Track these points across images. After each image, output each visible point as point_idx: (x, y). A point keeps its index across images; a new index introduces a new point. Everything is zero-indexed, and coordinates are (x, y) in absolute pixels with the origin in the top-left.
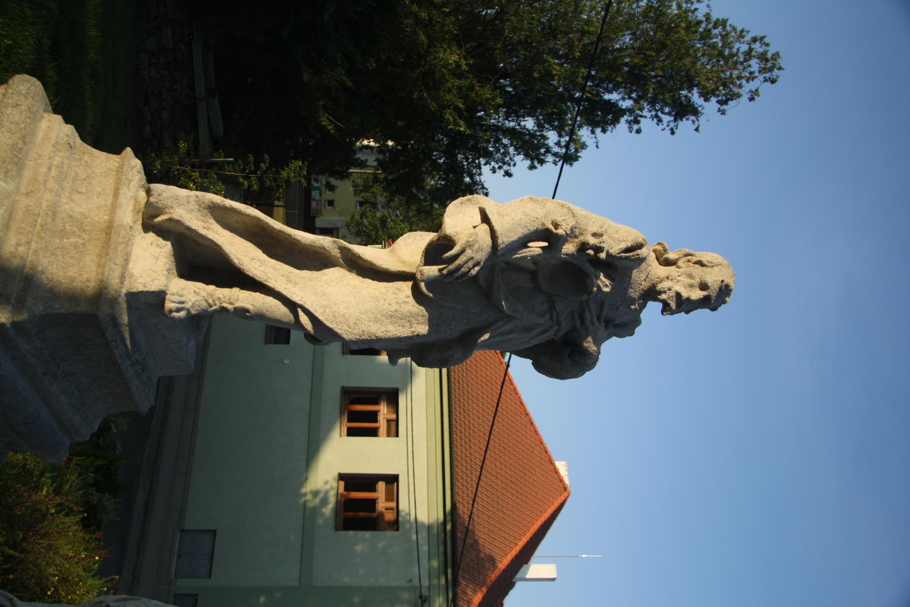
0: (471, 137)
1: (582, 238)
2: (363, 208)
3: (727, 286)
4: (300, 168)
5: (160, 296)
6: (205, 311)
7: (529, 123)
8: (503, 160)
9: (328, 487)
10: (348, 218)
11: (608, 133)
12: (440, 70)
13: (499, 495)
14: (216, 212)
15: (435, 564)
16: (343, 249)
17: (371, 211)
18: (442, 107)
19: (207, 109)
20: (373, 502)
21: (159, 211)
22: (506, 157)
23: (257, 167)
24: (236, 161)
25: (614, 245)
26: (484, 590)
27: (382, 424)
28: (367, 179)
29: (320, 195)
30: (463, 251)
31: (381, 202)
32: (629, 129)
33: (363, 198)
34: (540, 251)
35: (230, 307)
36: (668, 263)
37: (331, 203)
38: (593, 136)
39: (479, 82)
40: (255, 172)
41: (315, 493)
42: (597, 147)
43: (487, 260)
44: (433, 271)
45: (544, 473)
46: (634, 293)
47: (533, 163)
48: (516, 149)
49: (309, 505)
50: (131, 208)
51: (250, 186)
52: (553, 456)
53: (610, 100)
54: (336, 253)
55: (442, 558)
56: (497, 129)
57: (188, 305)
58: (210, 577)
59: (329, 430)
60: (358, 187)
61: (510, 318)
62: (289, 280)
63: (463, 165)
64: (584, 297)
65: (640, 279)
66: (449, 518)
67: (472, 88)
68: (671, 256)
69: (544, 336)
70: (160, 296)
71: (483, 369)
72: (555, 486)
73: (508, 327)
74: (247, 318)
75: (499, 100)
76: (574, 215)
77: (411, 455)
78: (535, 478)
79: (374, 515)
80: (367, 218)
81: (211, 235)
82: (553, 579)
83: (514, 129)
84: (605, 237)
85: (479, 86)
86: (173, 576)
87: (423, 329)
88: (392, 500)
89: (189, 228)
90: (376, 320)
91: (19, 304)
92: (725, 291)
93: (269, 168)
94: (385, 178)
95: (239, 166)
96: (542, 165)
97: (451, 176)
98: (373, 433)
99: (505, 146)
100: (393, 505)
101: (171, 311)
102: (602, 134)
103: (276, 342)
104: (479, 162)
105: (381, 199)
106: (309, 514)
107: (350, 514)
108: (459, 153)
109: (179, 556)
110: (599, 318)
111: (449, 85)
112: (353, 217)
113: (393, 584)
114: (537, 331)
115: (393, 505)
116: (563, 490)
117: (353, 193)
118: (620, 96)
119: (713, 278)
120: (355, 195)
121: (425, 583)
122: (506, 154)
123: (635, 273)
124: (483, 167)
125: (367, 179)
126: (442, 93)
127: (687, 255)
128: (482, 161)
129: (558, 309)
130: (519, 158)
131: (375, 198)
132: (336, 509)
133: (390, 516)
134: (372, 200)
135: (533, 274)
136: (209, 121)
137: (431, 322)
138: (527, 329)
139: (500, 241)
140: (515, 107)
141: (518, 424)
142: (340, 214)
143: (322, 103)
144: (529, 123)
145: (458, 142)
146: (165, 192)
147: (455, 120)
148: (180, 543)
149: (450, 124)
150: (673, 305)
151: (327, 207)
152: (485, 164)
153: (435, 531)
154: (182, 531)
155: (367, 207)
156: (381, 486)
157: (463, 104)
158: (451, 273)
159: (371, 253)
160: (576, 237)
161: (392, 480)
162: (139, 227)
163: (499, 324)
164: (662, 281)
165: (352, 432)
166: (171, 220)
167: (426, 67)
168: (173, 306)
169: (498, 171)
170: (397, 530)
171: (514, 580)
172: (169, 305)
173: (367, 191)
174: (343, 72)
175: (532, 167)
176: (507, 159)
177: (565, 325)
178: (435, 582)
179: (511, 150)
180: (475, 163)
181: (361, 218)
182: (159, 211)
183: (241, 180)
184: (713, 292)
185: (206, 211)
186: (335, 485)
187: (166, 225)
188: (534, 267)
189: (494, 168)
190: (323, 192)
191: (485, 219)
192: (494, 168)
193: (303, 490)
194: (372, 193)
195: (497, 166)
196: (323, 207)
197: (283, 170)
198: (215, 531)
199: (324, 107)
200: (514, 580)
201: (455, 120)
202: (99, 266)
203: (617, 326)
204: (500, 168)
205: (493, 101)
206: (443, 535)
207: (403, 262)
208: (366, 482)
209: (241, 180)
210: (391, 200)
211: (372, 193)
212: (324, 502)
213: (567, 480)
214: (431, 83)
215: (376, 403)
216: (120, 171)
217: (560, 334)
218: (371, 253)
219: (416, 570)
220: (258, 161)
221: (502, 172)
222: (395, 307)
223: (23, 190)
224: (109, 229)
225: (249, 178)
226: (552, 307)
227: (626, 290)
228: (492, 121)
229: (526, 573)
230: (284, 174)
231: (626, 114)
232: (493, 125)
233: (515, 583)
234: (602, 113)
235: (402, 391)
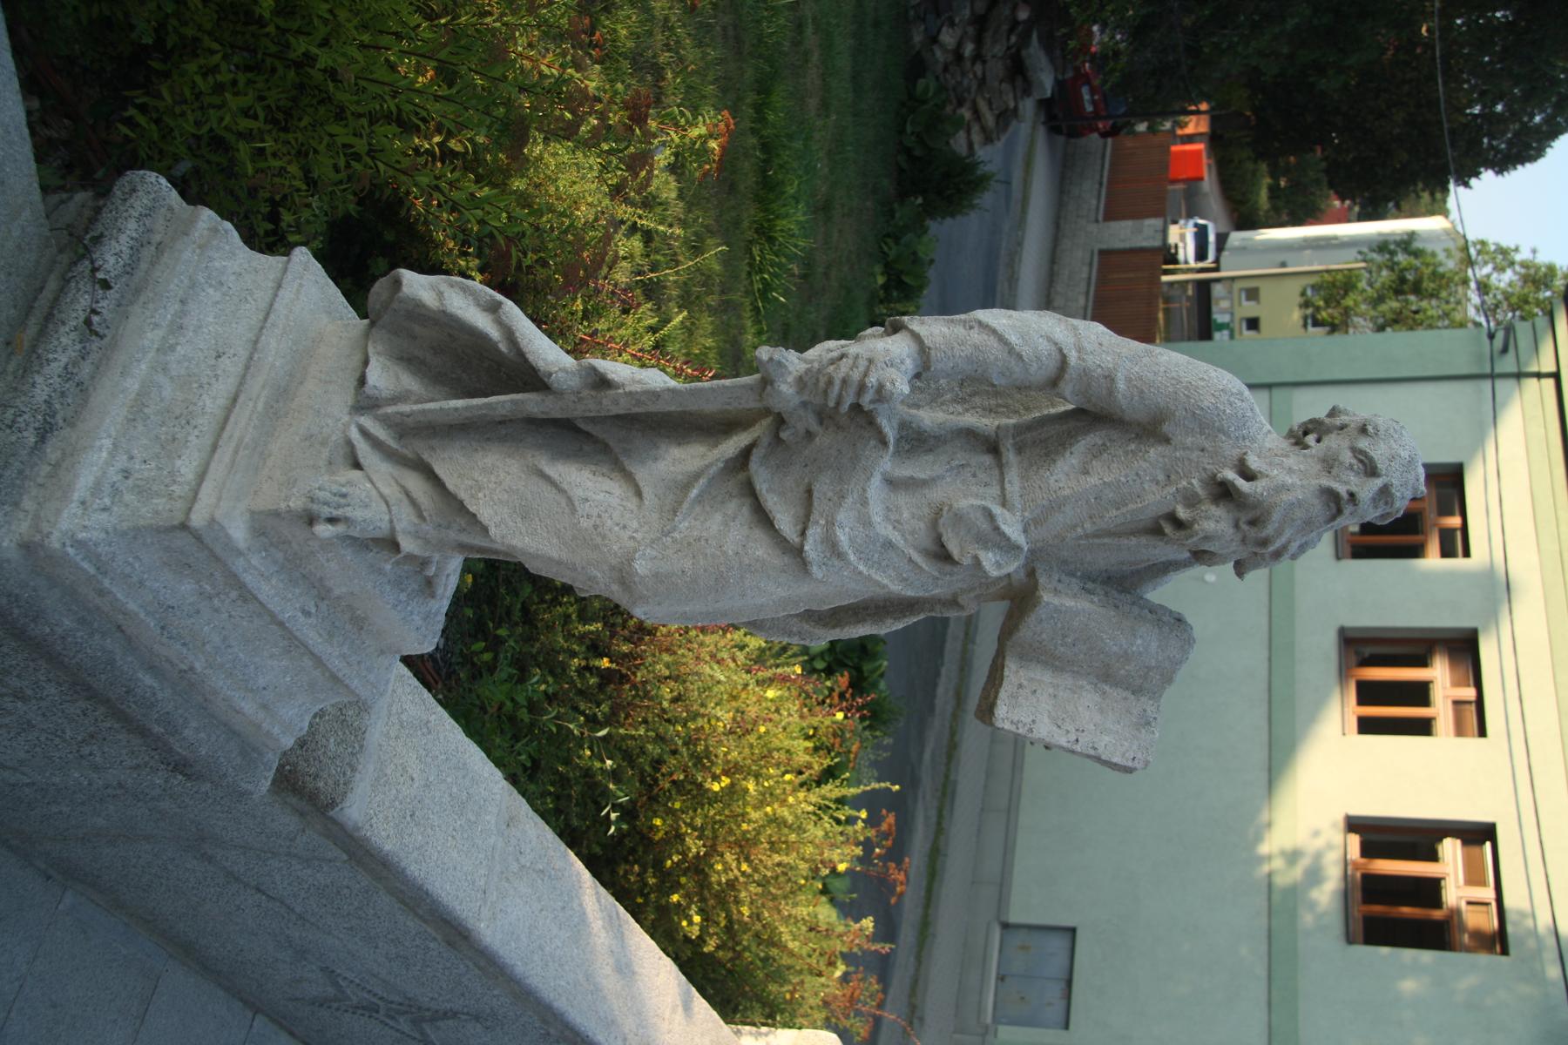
9: (1319, 843)
20: (1430, 890)
27: (1441, 708)
41: (1293, 856)
49: (1280, 881)
58: (1067, 1027)
59: (1314, 714)
79: (1437, 914)
86: (989, 1020)
98: (1423, 727)
107: (1377, 909)
109: (1001, 978)
115: (1488, 894)
132: (1346, 894)
148: (1000, 951)
154: (1006, 926)
156: (1450, 848)
161: (1479, 835)
165: (1368, 726)
193: (1264, 849)
198: (1073, 931)
212: (1314, 875)
215: (1423, 662)
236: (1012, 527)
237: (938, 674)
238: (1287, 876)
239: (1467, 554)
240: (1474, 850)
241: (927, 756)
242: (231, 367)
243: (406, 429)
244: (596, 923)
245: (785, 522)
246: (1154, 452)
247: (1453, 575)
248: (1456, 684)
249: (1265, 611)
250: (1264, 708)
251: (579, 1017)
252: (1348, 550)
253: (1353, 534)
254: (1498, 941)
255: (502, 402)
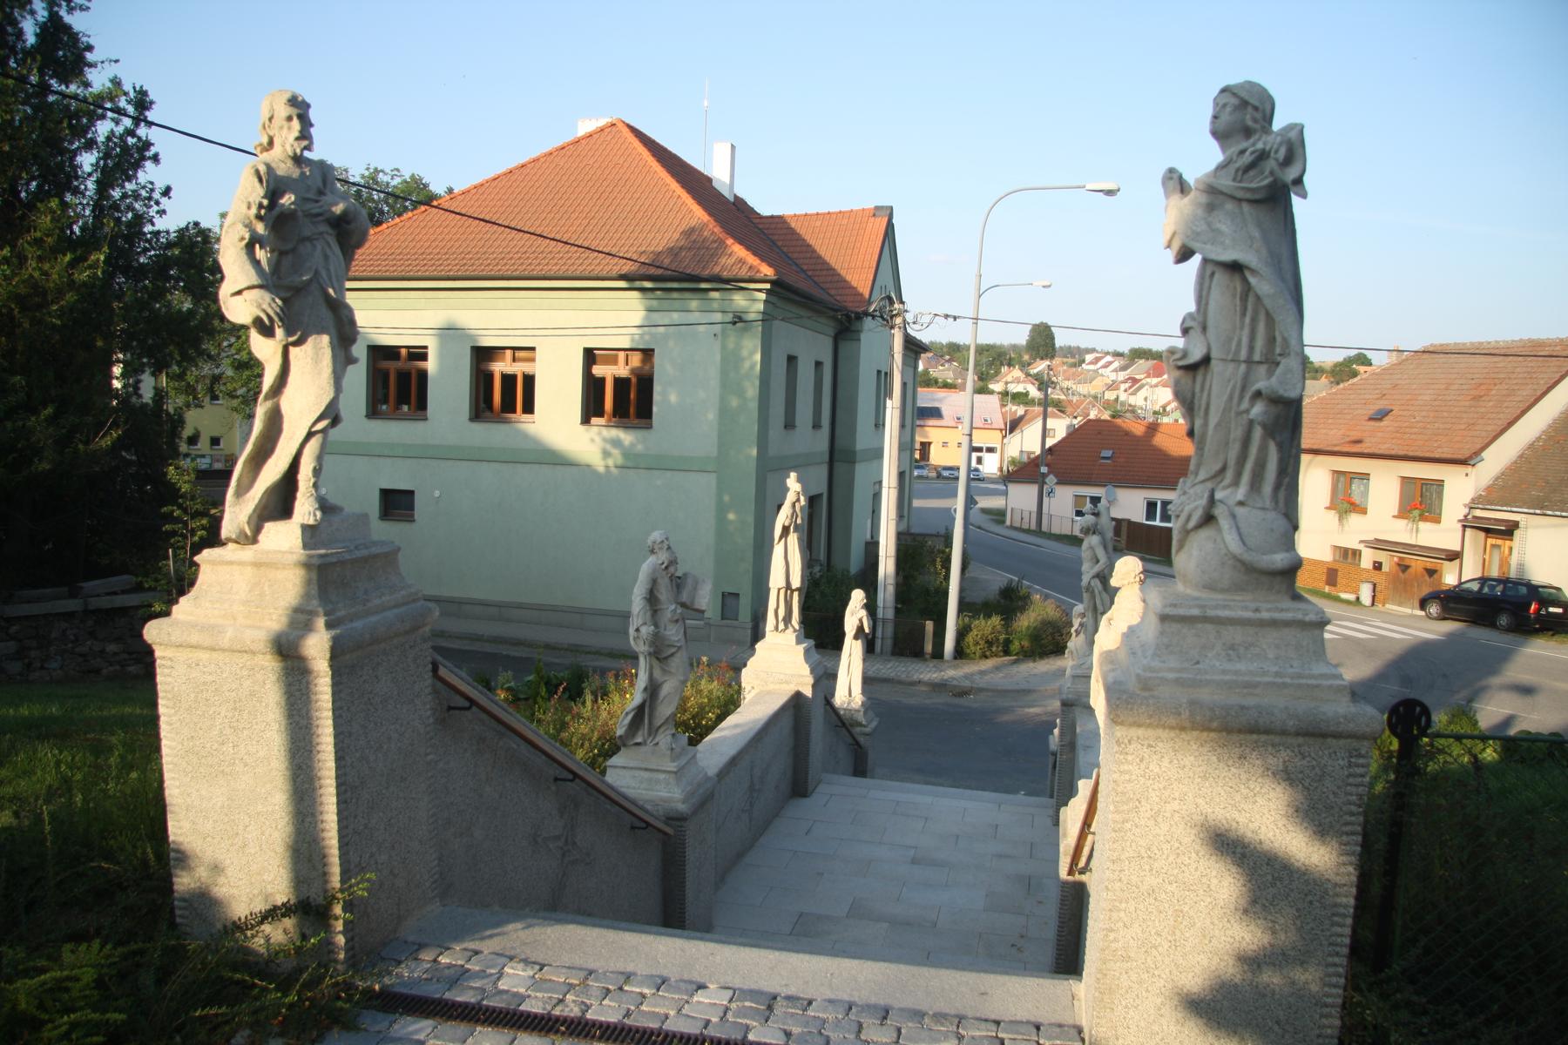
0: (112, 245)
1: (252, 218)
2: (221, 395)
3: (289, 101)
4: (177, 468)
5: (306, 528)
6: (316, 498)
7: (87, 160)
8: (146, 198)
9: (598, 439)
10: (236, 416)
11: (92, 41)
12: (14, 287)
13: (614, 216)
14: (240, 493)
15: (694, 304)
16: (266, 398)
17: (225, 384)
18: (72, 284)
19: (98, 596)
20: (620, 383)
21: (242, 532)
22: (140, 195)
23: (178, 520)
24: (172, 546)
25: (257, 193)
26: (730, 241)
27: (518, 369)
28: (176, 389)
29: (203, 456)
30: (264, 311)
31: (210, 369)
32: (84, 10)
33: (205, 396)
34: (263, 251)
35: (313, 480)
36: (271, 143)
37: (215, 441)
38: (99, 65)
39: (29, 231)
40: (186, 523)
41: (606, 454)
42: (117, 61)
43: (271, 293)
44: (279, 332)
45: (590, 154)
46: (296, 173)
47: (149, 158)
48: (129, 179)
49: (620, 461)
50: (240, 552)
51: (203, 528)
52: (569, 138)
53: (37, 35)
54: (269, 404)
55: (687, 295)
56: (102, 206)
57: (312, 509)
59: (526, 436)
60: (188, 402)
61: (317, 272)
62: (291, 438)
63: (155, 255)
64: (300, 213)
65: (285, 169)
66: (638, 284)
67: (38, 242)
68: (265, 140)
69: (332, 244)
70: (306, 528)
71: (446, 231)
72: (609, 138)
73: (324, 273)
74: (320, 469)
75: (54, 203)
76: (234, 224)
77: (559, 331)
78: (597, 165)
79: (634, 380)
80: (235, 390)
81: (259, 495)
82: (733, 147)
83: (98, 182)
84: (251, 200)
85: (35, 231)
86: (702, 623)
87: (325, 339)
88: (616, 357)
89: (254, 511)
90: (319, 373)
91: (312, 614)
92: (294, 101)
93: (180, 507)
94: (179, 364)
95: (179, 542)
96: (153, 144)
97: (172, 272)
98: (529, 380)
99: (125, 196)
100: (622, 355)
101: (316, 520)
102: (95, 51)
103: (411, 508)
104: (150, 233)
105: (207, 369)
106: (632, 463)
107: (632, 410)
108: (138, 261)
110: (317, 201)
111: (36, 274)
112: (235, 409)
113: (718, 357)
114: (328, 250)
115: (622, 355)
116: (614, 129)
117: (199, 410)
118: (28, 17)
119: (283, 110)
120: (202, 407)
121: (718, 317)
122: (136, 196)
123: (280, 173)
124: (156, 228)
125: (176, 389)
126: (52, 285)
127: (264, 128)
128: (148, 228)
129: (309, 234)
130: (142, 177)
131: (204, 376)
132: (626, 427)
133: (636, 360)
134: (208, 381)
135: (282, 254)
136: (115, 593)
137: (320, 331)
138: (326, 257)
139: (256, 283)
140: (63, 179)
141: (523, 185)
142: (230, 428)
143: (81, 446)
144: (87, 160)
145: (121, 261)
146: (227, 529)
147: (90, 267)
149: (95, 274)
150: (305, 143)
151: (222, 446)
152: (153, 224)
153: (655, 303)
155: (220, 388)
156: (598, 370)
157: (65, 255)
158: (281, 320)
159: (268, 380)
160: (251, 222)
161: (590, 356)
162: (255, 547)
163: (321, 281)
164: (285, 150)
165: (529, 408)
166: (248, 523)
167: (13, 306)
168: (312, 518)
169: (162, 207)
170: (653, 350)
171: (732, 199)
172: (311, 522)
173: (195, 389)
174: (33, 419)
175: (156, 159)
176: (144, 193)
177: (324, 228)
178: (715, 305)
179: (129, 186)
180: (151, 239)
181: (237, 397)
182: (242, 532)
183: (196, 538)
184: (294, 111)
185: (241, 500)
186: (595, 429)
187: (252, 527)
188: (280, 255)
189: (158, 212)
190: (200, 453)
191: (239, 293)
192: (158, 212)
193: (601, 469)
194: (197, 382)
195: (155, 208)
196: (220, 452)
197: (180, 489)
199: (87, 443)
200: (732, 199)
201: (90, 267)
202: (284, 568)
203: (324, 182)
204: (157, 203)
205: (55, 212)
206: (658, 293)
207: (275, 353)
208: (593, 389)
209: (196, 538)
210: (210, 357)
211: (197, 382)
212: (616, 443)
213: (602, 122)
214: (36, 299)
215: (490, 376)
216: (213, 563)
217: (330, 231)
218: (268, 380)
219: (701, 328)
220: (169, 518)
221: (164, 200)
222: (309, 360)
223: (232, 622)
224: (257, 565)
225: (193, 530)
226: (309, 239)
227: (294, 180)
228: (87, 212)
229: (725, 183)
230: (185, 488)
231: (57, 13)
232: (93, 211)
233: (736, 197)
234: (59, 49)
235: (476, 341)
236: (673, 607)
237: (508, 656)
238: (617, 457)
239: (426, 347)
240: (598, 359)
241: (557, 661)
242: (637, 773)
243: (650, 735)
244: (722, 734)
245: (673, 650)
246: (659, 580)
247: (442, 356)
248: (503, 360)
249: (458, 463)
250: (519, 465)
251: (751, 734)
252: (419, 413)
253: (409, 409)
254: (648, 353)
255: (647, 710)
